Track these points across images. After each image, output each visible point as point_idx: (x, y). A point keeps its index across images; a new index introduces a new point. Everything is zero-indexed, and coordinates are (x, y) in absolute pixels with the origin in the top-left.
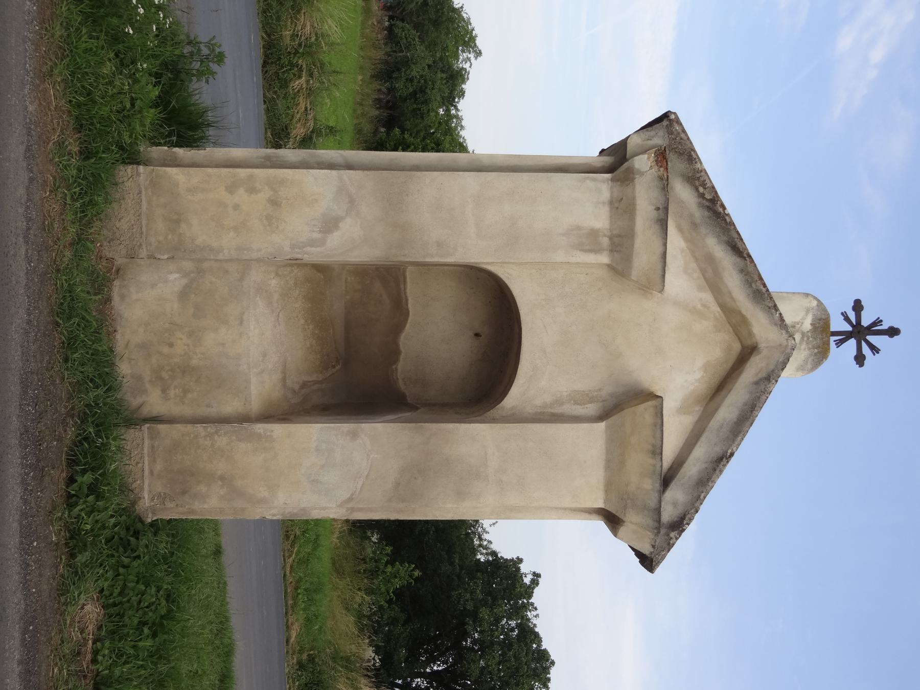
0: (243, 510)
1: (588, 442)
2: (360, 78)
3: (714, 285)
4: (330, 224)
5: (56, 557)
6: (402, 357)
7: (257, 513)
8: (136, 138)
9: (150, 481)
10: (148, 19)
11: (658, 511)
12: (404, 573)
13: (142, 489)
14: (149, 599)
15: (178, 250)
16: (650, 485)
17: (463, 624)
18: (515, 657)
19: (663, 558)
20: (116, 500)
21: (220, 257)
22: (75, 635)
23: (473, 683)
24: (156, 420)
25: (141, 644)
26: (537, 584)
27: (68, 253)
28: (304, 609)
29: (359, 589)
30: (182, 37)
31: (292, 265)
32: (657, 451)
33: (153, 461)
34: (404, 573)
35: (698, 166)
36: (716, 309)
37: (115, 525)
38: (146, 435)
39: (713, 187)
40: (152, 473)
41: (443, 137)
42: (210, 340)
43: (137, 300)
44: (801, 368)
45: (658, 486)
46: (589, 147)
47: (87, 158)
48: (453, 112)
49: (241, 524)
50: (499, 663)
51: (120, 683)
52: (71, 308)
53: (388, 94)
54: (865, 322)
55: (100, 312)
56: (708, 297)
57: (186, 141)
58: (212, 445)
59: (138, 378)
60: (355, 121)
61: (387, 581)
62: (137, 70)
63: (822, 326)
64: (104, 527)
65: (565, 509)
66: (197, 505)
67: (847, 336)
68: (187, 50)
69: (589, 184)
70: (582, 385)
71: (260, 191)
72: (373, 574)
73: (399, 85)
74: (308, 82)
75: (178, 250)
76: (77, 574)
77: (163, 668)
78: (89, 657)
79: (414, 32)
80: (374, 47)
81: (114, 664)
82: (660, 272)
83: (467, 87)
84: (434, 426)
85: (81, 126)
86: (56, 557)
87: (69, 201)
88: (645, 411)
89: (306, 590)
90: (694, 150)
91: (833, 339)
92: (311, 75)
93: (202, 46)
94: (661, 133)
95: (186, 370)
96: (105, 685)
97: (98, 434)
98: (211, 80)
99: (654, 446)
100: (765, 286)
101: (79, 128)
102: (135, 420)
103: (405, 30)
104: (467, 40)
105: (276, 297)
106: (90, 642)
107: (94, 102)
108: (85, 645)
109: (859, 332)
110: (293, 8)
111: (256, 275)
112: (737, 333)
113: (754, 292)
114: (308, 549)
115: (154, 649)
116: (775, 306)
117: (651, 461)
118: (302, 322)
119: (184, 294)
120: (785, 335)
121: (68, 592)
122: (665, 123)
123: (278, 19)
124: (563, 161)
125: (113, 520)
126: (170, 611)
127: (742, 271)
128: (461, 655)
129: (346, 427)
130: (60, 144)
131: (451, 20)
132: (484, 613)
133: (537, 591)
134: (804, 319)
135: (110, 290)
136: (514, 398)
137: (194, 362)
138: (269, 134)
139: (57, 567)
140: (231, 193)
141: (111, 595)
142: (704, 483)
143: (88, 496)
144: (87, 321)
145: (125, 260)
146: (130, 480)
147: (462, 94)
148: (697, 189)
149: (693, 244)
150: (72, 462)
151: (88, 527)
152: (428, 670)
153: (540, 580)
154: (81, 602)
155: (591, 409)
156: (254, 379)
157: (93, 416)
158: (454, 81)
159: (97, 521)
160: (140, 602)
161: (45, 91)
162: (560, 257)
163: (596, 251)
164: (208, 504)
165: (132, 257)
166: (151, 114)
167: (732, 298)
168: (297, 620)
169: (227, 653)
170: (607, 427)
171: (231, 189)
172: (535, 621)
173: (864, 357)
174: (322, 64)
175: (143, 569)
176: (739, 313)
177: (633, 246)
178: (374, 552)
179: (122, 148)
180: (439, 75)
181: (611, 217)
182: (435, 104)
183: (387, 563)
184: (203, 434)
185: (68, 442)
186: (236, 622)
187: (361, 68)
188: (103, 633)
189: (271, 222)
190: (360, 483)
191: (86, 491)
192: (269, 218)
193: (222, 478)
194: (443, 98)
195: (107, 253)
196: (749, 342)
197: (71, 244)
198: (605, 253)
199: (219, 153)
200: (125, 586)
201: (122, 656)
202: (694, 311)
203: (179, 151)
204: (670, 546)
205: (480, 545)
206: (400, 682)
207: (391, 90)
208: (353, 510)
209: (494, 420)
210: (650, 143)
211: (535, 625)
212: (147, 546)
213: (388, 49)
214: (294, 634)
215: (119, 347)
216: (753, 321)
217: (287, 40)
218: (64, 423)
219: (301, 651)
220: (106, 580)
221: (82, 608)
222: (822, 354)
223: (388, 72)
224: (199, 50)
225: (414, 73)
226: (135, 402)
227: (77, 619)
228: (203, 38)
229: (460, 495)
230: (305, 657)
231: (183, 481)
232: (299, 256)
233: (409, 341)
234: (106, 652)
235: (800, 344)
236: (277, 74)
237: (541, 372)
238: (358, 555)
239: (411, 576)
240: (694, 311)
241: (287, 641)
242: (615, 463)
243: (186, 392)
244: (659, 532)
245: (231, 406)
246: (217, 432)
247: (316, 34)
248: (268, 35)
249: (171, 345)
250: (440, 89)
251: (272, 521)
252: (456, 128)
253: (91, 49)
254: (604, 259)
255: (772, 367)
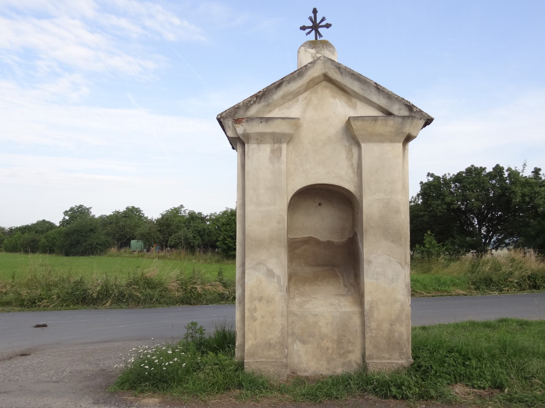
0: (407, 315)
1: (371, 151)
2: (194, 261)
3: (296, 95)
4: (270, 273)
5: (433, 405)
6: (331, 240)
7: (408, 309)
8: (232, 363)
9: (395, 359)
10: (180, 357)
11: (403, 117)
12: (429, 238)
13: (397, 364)
14: (452, 361)
15: (283, 345)
16: (391, 122)
17: (454, 210)
18: (470, 184)
19: (426, 114)
20: (404, 376)
21: (286, 325)
22: (471, 397)
23: (483, 203)
24: (363, 356)
25: (474, 366)
26: (433, 174)
27: (287, 396)
28: (449, 287)
29: (438, 260)
30: (184, 341)
31: (289, 291)
32: (375, 119)
33: (383, 358)
34: (429, 238)
35: (241, 104)
36: (306, 94)
37: (416, 377)
38: (371, 361)
39: (251, 97)
40: (389, 359)
41: (227, 222)
42: (325, 330)
43: (307, 364)
44: (333, 53)
45: (391, 118)
46: (234, 155)
47: (242, 386)
48: (208, 217)
49: (414, 316)
50: (473, 192)
51: (495, 376)
52: (312, 395)
53: (200, 247)
54: (311, 24)
55: (313, 381)
56: (301, 98)
57: (232, 341)
58: (376, 329)
59: (344, 364)
60: (214, 263)
61: (433, 246)
62: (201, 362)
63: (313, 44)
64: (417, 382)
65: (403, 161)
66: (405, 337)
67: (317, 32)
68: (190, 339)
69: (250, 154)
70: (344, 155)
71: (255, 306)
72: (429, 254)
73: (197, 243)
74: (198, 285)
75: (283, 345)
76: (441, 396)
77: (486, 355)
78: (482, 391)
79: (173, 236)
80: (180, 254)
81: (485, 379)
82: (290, 120)
83: (197, 212)
84: (365, 224)
85: (227, 388)
86: (433, 405)
87: (262, 395)
88: (356, 125)
89: (439, 286)
90: (234, 106)
91: (318, 39)
92: (195, 283)
93: (189, 332)
94: (227, 122)
95: (339, 342)
96: (496, 384)
97: (371, 384)
98: (203, 328)
99: (372, 120)
100: (296, 71)
101: (228, 389)
102: (364, 367)
103: (172, 240)
104: (176, 212)
105: (304, 299)
106: (474, 390)
107: (217, 382)
108: (476, 392)
109: (315, 27)
110: (165, 291)
111: (294, 308)
112: (318, 83)
113: (299, 76)
114: (418, 285)
115: (476, 360)
116: (305, 66)
117: (380, 121)
118: (315, 287)
119: (304, 342)
120: (319, 61)
121: (450, 400)
122: (222, 120)
123: (170, 298)
124: (240, 166)
125: (414, 378)
126: (457, 351)
127: (289, 82)
128: (469, 210)
129: (366, 266)
130: (236, 398)
131: (167, 219)
132: (448, 199)
133: (436, 174)
134: (310, 53)
135: (302, 376)
136: (349, 185)
137: (336, 338)
138: (223, 302)
139: (438, 405)
140: (256, 319)
141: (450, 379)
142: (389, 96)
143: (402, 389)
144: (318, 387)
145: (288, 369)
146: (393, 369)
147: (200, 214)
148: (252, 104)
149: (277, 105)
150: (386, 397)
151: (417, 389)
152: (477, 226)
153: (431, 173)
154: (455, 394)
155: (355, 150)
156: (343, 310)
157: (363, 386)
158: (194, 217)
159: (414, 385)
160: (453, 366)
161: (212, 404)
162: (284, 167)
163: (280, 150)
164: (404, 332)
165: (287, 366)
166: (221, 356)
167: (302, 86)
168: (454, 290)
169: (473, 324)
170: (363, 142)
171: (254, 319)
172: (451, 175)
173: (327, 24)
174: (191, 278)
175: (437, 364)
176: (308, 83)
177: (278, 133)
178: (419, 253)
179: (237, 370)
180: (192, 224)
181: (265, 143)
182: (205, 226)
183: (424, 247)
184: (370, 334)
185: (376, 398)
186: (459, 320)
187: (189, 260)
188: (470, 384)
189: (269, 301)
190: (393, 259)
191: (400, 390)
192: (268, 302)
193: (391, 325)
194: (202, 223)
195: (285, 378)
196: (322, 78)
197: (282, 394)
198: (282, 145)
199: (238, 324)
200: (446, 373)
201: (480, 375)
202: (308, 104)
203: (237, 343)
204: (420, 111)
205: (414, 202)
206: (483, 240)
207: (199, 247)
208: (406, 263)
209: (361, 196)
210: (231, 126)
211: (454, 175)
212: (426, 362)
213: (180, 247)
214: (461, 292)
215: (328, 373)
216: (312, 76)
217: (180, 294)
218: (367, 400)
219: (470, 289)
220: (443, 381)
221: (458, 393)
222: (326, 44)
223: (191, 248)
224: (190, 333)
225: (191, 236)
226: (355, 366)
227: (463, 396)
228: (185, 331)
229: (397, 211)
230: (472, 287)
231: (393, 344)
232: (285, 288)
233: (323, 237)
234: (479, 382)
235: (321, 54)
236: (195, 299)
237: (340, 176)
238: (420, 261)
239: (430, 235)
240: (308, 104)
241: (465, 295)
242: (381, 138)
243: (350, 342)
244: (414, 116)
245: (356, 321)
246: (369, 327)
247: (177, 280)
248: (178, 302)
249: (328, 348)
250: (198, 224)
251: (412, 301)
252: (215, 216)
253: (193, 383)
254: (284, 146)
255: (333, 67)
